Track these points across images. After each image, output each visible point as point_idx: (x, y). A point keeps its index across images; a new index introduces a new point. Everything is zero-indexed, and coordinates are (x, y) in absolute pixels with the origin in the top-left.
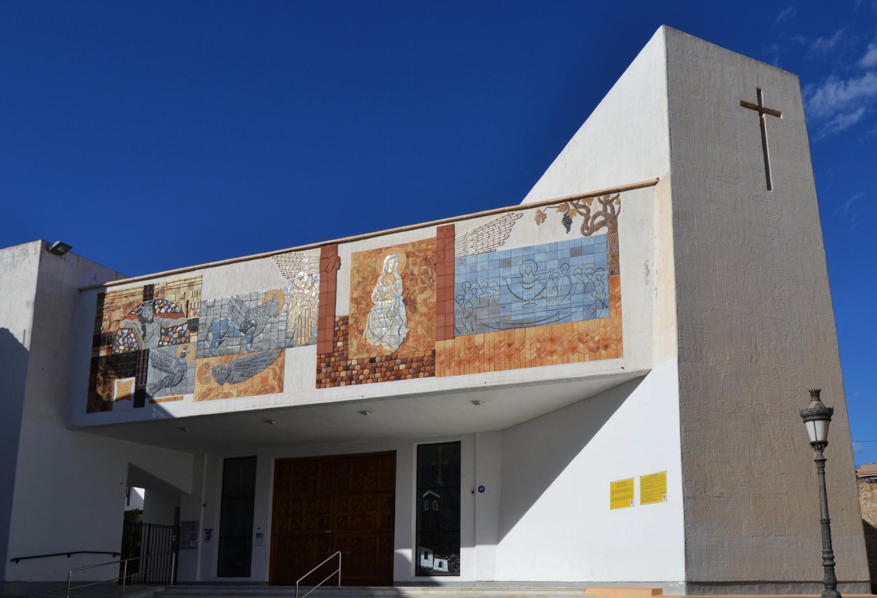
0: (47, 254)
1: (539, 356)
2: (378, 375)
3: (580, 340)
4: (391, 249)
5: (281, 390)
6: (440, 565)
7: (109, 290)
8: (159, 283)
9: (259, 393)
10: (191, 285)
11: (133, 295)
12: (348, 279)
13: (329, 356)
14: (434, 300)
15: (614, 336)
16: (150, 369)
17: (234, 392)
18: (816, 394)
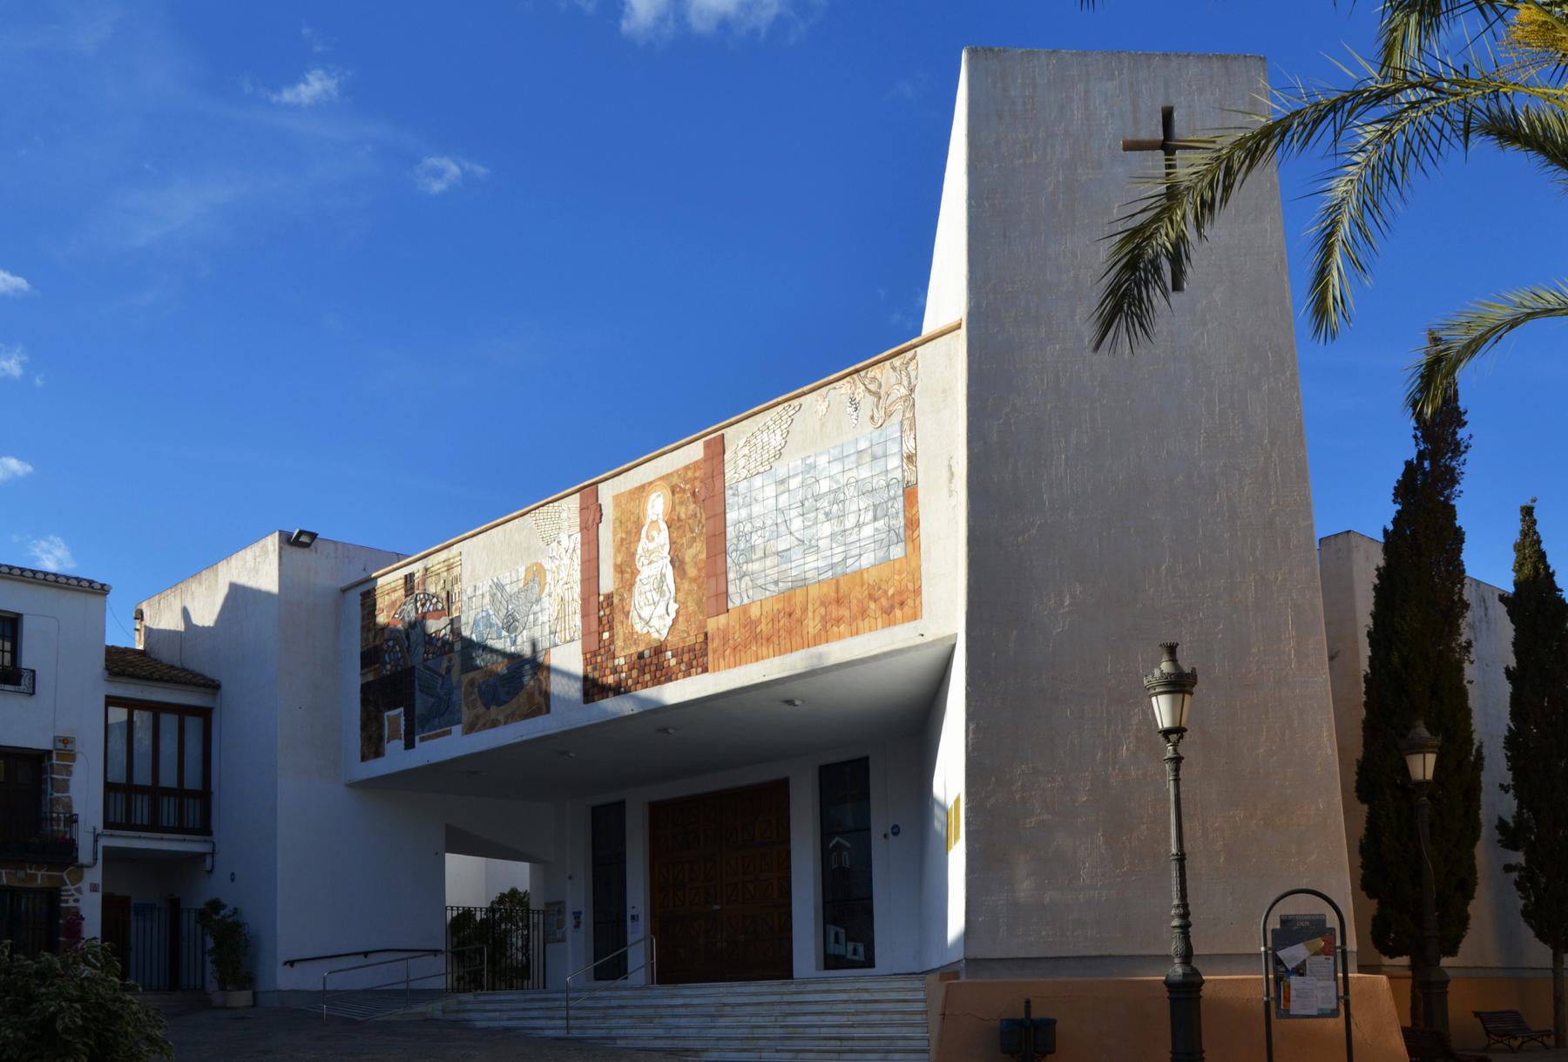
0: (288, 549)
1: (824, 627)
2: (647, 677)
3: (871, 597)
4: (649, 484)
5: (548, 711)
6: (855, 952)
7: (380, 581)
8: (417, 568)
9: (526, 716)
10: (449, 568)
11: (394, 590)
12: (610, 535)
13: (595, 654)
14: (703, 556)
15: (911, 587)
16: (418, 694)
17: (501, 718)
18: (1172, 650)
